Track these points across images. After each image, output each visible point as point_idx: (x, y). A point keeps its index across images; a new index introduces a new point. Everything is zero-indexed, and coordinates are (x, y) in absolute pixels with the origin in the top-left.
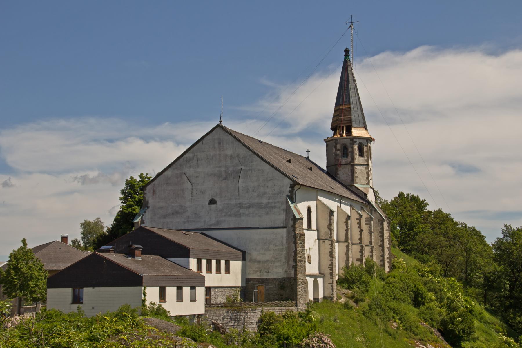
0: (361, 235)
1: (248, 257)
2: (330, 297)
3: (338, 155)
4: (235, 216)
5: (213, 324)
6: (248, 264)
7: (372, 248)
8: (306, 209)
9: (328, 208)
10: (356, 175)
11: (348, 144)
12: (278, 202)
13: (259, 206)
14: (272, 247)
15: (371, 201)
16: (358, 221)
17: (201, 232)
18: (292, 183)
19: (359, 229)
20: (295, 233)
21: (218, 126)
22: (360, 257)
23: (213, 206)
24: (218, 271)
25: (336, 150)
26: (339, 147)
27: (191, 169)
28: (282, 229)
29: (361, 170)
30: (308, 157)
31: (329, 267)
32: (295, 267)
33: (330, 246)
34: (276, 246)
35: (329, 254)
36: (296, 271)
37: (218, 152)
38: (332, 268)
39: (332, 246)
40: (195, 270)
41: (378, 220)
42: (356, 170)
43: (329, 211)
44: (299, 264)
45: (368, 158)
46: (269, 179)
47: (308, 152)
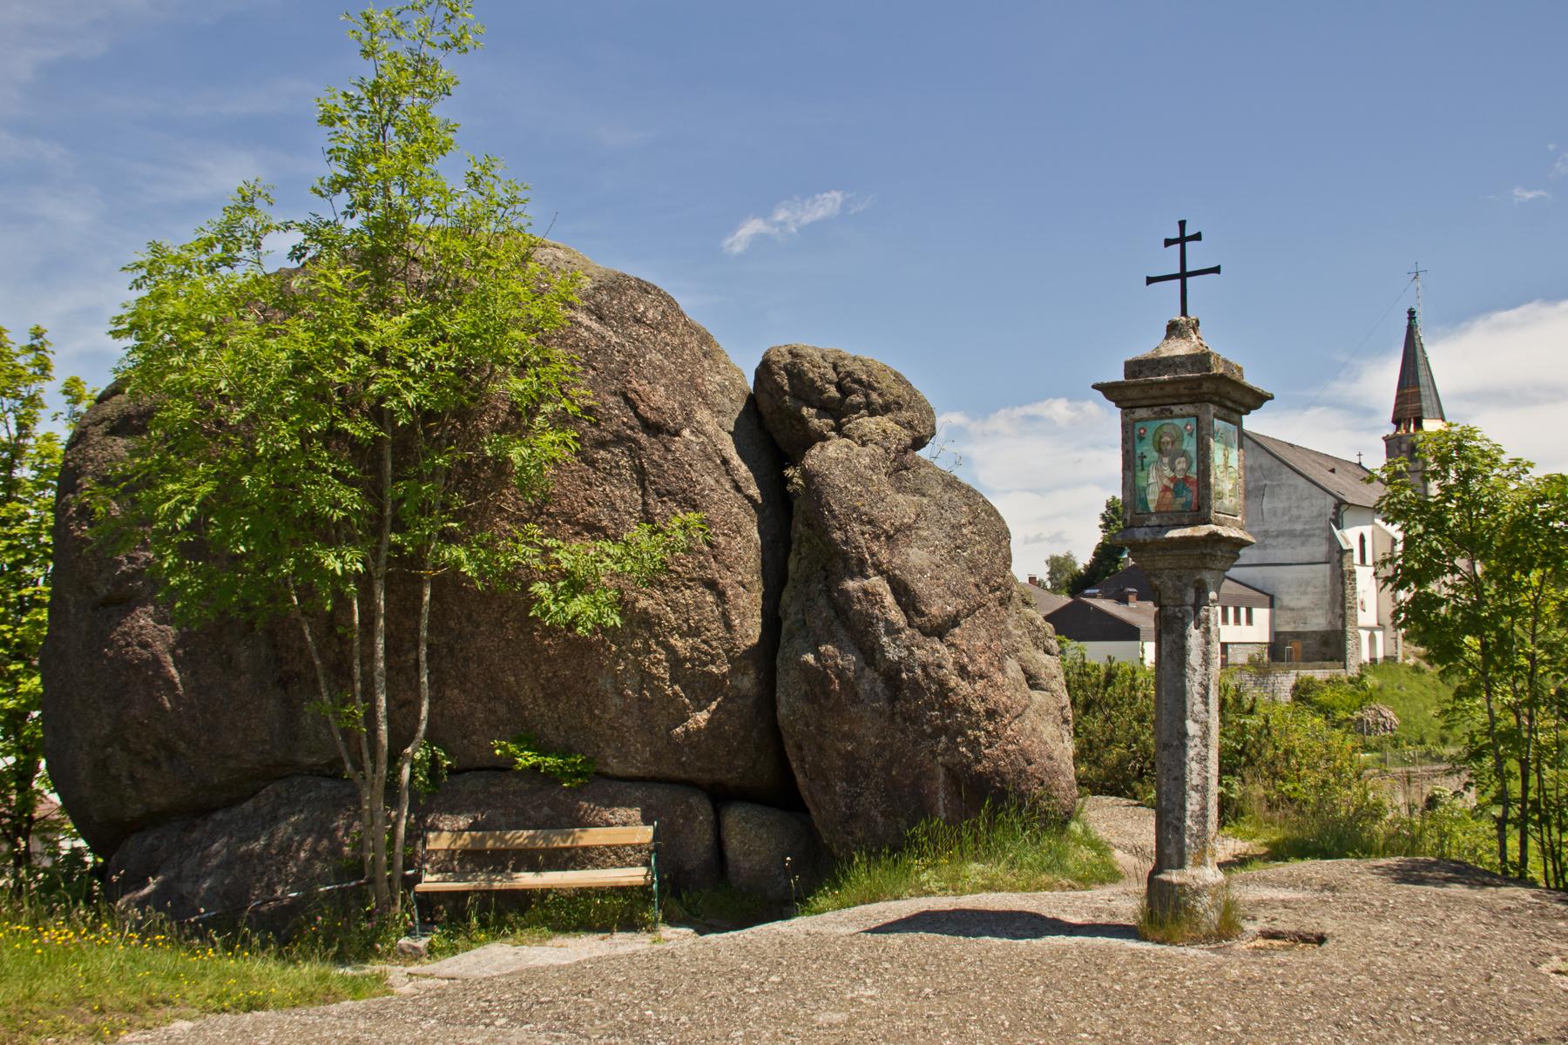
1: (1277, 603)
13: (1292, 534)
14: (1310, 589)
24: (1237, 621)
32: (1343, 617)
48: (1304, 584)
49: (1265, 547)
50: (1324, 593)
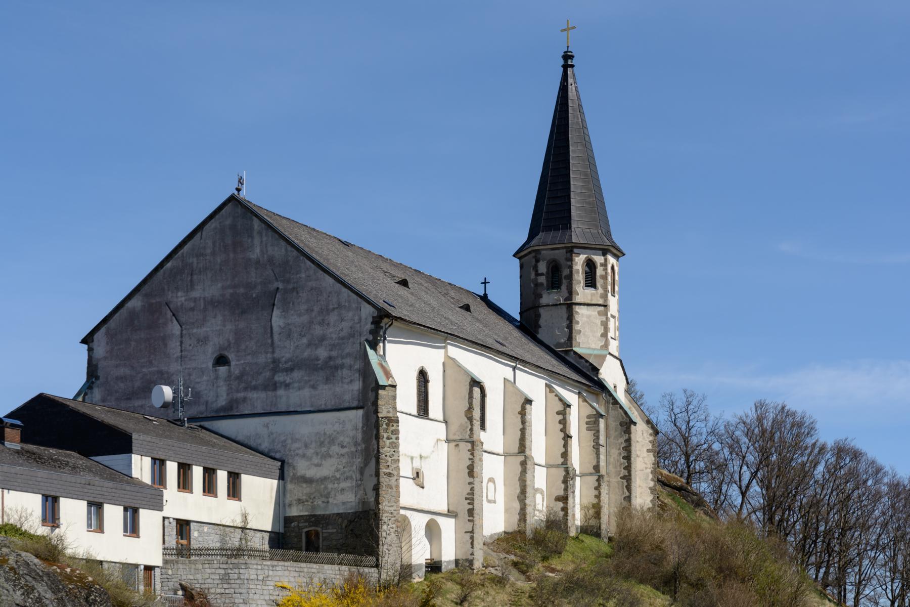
0: (566, 446)
1: (289, 473)
2: (467, 560)
3: (542, 284)
4: (265, 388)
5: (183, 588)
6: (290, 486)
7: (599, 480)
8: (415, 374)
9: (466, 372)
10: (576, 327)
11: (562, 261)
12: (349, 355)
13: (311, 366)
14: (335, 449)
15: (611, 387)
16: (561, 417)
17: (198, 424)
18: (376, 314)
19: (562, 435)
20: (378, 417)
21: (232, 199)
22: (561, 493)
23: (223, 370)
24: (209, 488)
25: (537, 274)
26: (542, 267)
27: (180, 294)
28: (354, 412)
29: (589, 317)
30: (485, 295)
31: (466, 499)
32: (377, 488)
33: (468, 455)
34: (343, 447)
35: (467, 471)
36: (378, 495)
37: (232, 255)
38: (473, 499)
39: (472, 454)
40: (147, 479)
41: (621, 425)
42: (577, 318)
43: (469, 380)
44: (383, 479)
45: (606, 291)
46: (331, 307)
47: (485, 283)
48: (325, 442)
49: (275, 387)
50: (353, 455)
